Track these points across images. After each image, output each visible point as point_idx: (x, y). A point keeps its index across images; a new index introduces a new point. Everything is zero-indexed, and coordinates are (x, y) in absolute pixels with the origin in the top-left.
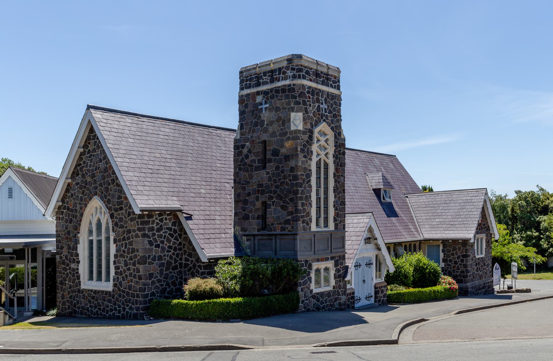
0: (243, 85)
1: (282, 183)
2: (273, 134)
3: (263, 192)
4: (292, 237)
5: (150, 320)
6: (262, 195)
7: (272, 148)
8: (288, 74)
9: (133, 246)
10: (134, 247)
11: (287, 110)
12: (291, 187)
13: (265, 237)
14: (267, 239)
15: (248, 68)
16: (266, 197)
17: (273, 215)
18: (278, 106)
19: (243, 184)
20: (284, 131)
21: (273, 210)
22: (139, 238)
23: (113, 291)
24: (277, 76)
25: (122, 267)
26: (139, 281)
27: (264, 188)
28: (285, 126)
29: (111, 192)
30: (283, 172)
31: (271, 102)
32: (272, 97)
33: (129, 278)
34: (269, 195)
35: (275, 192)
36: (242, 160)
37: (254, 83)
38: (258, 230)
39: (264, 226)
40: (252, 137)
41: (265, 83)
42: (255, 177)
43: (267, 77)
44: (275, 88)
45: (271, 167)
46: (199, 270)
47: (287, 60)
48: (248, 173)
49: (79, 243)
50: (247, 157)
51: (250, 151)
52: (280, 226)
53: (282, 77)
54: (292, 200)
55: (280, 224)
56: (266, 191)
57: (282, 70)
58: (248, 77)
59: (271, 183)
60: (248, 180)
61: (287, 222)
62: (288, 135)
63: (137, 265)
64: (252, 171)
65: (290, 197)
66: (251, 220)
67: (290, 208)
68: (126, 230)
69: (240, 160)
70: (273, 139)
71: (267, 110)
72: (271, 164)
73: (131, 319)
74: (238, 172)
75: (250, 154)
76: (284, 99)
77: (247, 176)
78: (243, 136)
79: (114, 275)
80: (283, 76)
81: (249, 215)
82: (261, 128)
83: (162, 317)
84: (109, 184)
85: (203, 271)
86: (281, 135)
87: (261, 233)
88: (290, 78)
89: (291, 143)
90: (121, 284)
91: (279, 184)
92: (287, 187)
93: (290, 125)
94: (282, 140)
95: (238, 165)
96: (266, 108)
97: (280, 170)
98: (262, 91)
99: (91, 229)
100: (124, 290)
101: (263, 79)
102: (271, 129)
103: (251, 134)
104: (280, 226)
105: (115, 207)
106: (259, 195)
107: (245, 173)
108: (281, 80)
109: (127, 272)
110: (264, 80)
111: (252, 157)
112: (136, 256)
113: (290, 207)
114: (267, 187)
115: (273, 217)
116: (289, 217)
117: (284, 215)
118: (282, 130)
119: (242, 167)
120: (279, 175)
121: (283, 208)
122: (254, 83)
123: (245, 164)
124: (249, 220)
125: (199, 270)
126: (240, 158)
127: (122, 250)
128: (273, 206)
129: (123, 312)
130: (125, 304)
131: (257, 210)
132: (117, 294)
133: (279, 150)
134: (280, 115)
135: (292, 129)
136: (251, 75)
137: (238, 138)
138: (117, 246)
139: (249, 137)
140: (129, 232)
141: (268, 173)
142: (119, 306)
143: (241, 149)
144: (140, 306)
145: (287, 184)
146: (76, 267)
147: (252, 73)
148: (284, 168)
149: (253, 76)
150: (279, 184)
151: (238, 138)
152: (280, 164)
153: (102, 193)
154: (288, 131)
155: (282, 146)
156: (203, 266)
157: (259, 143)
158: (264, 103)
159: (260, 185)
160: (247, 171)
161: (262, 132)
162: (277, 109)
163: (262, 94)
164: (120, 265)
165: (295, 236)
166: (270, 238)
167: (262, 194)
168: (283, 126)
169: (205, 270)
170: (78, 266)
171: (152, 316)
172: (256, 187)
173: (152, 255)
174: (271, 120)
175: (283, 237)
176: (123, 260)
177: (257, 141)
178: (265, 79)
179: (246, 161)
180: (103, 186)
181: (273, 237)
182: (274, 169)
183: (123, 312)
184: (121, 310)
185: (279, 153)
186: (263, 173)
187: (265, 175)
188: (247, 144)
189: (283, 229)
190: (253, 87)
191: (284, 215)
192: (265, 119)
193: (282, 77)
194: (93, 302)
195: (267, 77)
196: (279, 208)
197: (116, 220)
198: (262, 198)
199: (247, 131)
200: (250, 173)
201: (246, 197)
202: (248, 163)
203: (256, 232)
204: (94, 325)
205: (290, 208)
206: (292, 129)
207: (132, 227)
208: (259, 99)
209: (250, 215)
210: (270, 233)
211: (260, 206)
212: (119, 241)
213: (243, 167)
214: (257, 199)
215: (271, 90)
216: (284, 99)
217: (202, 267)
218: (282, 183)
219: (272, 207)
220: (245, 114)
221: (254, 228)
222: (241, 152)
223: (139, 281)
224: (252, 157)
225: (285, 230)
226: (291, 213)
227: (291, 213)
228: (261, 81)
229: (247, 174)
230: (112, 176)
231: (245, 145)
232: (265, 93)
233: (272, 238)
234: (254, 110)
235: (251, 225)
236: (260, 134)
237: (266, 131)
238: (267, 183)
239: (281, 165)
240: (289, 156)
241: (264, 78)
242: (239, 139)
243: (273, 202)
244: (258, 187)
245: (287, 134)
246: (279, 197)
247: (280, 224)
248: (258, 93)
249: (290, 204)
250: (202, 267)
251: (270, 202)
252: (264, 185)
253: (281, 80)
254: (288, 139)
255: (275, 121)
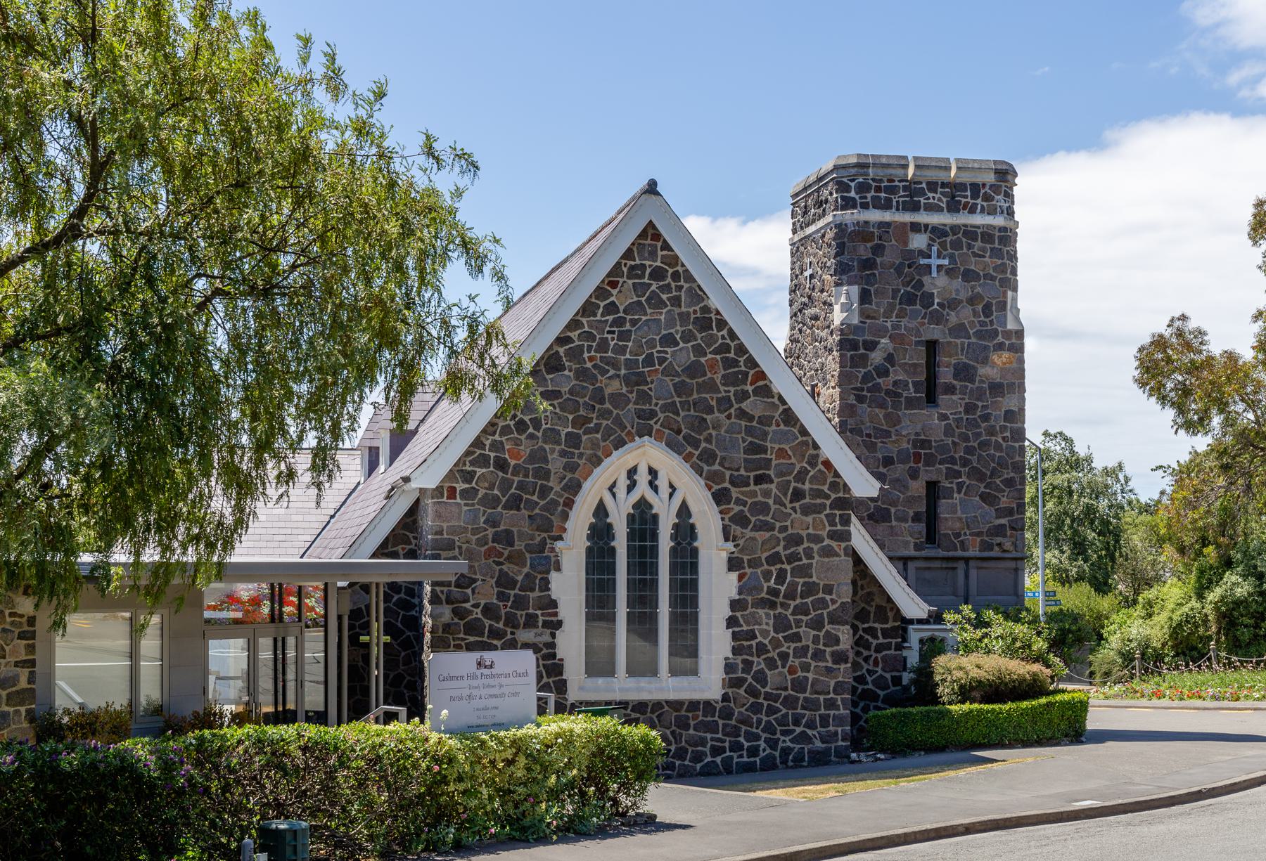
0: (866, 198)
1: (984, 445)
2: (959, 330)
3: (930, 460)
4: (1012, 564)
5: (877, 759)
6: (928, 466)
7: (953, 362)
8: (999, 204)
9: (811, 577)
10: (814, 579)
11: (997, 283)
12: (1007, 455)
13: (937, 564)
14: (942, 568)
15: (884, 161)
16: (939, 471)
17: (959, 514)
18: (973, 267)
19: (869, 436)
20: (989, 328)
21: (958, 501)
22: (838, 559)
23: (725, 698)
24: (969, 200)
25: (765, 633)
26: (835, 666)
27: (933, 451)
28: (993, 317)
29: (714, 433)
30: (986, 418)
31: (951, 257)
32: (957, 245)
33: (793, 661)
34: (947, 468)
35: (965, 463)
36: (867, 377)
37: (901, 199)
38: (918, 547)
39: (932, 536)
40: (896, 327)
41: (931, 208)
42: (905, 422)
43: (939, 195)
44: (965, 226)
45: (951, 404)
46: (871, 640)
47: (997, 172)
48: (883, 411)
49: (558, 569)
50: (883, 372)
51: (890, 358)
52: (979, 539)
53: (982, 206)
54: (1009, 483)
55: (979, 534)
56: (939, 457)
57: (983, 191)
58: (881, 181)
59: (953, 442)
60: (885, 428)
61: (999, 531)
62: (1000, 339)
63: (828, 627)
64: (896, 406)
65: (1006, 476)
66: (894, 523)
67: (1005, 502)
68: (781, 536)
69: (860, 376)
70: (958, 341)
71: (943, 273)
72: (954, 397)
73: (803, 766)
74: (852, 406)
75: (893, 366)
76: (991, 257)
77: (881, 416)
78: (868, 321)
79: (730, 655)
80: (985, 204)
81: (888, 510)
82: (924, 311)
83: (915, 750)
84: (710, 410)
85: (881, 640)
86: (979, 335)
87: (924, 553)
88: (1002, 212)
89: (1009, 358)
90: (761, 678)
91: (976, 445)
92: (998, 454)
93: (1005, 316)
94: (986, 348)
95: (852, 389)
96: (939, 267)
97: (979, 414)
98: (926, 226)
99: (882, 527)
100: (774, 692)
101: (928, 198)
102: (953, 319)
103: (894, 319)
104: (979, 539)
105: (736, 473)
106: (920, 465)
107: (877, 410)
108: (978, 210)
109: (786, 645)
110: (931, 201)
111: (897, 374)
112: (822, 604)
113: (1005, 499)
114: (943, 448)
115: (960, 519)
116: (1003, 521)
117: (987, 516)
118: (982, 324)
119: (865, 393)
120: (972, 424)
121: (984, 497)
122: (901, 199)
123: (876, 388)
124: (891, 521)
125: (871, 640)
126: (860, 372)
127: (765, 589)
128: (959, 492)
129: (768, 751)
130: (779, 728)
131: (911, 500)
132: (744, 705)
133: (975, 369)
134: (979, 290)
135: (1009, 327)
136: (894, 181)
137: (856, 321)
138: (740, 578)
139: (889, 324)
140: (795, 540)
141: (944, 417)
142: (752, 737)
143: (862, 351)
144: (840, 730)
145: (998, 447)
146: (547, 638)
147: (896, 176)
148: (989, 411)
149: (897, 183)
150: (976, 445)
151: (856, 321)
152: (978, 399)
153: (679, 432)
154: (1000, 329)
155: (985, 361)
156: (881, 629)
157: (918, 343)
158: (934, 254)
159: (925, 443)
160: (882, 406)
161: (926, 321)
162: (968, 276)
163: (925, 232)
164: (756, 627)
165: (1019, 562)
166: (950, 565)
167: (927, 464)
168: (987, 316)
169: (890, 640)
170: (553, 635)
171: (882, 751)
172: (910, 446)
173: (833, 602)
174: (954, 296)
175: (985, 564)
176: (767, 615)
177: (913, 338)
178: (934, 198)
179: (880, 381)
180: (682, 414)
181: (961, 566)
182: (961, 409)
183: (768, 751)
184: (759, 746)
185: (974, 375)
186: (930, 416)
187: (936, 422)
188: (883, 341)
189: (987, 546)
190: (898, 209)
191: (987, 516)
192: (935, 291)
193: (982, 206)
194: (759, 721)
195: (939, 195)
196: (977, 498)
197: (737, 509)
198: (927, 474)
199: (882, 310)
200: (890, 410)
201: (878, 467)
202: (884, 387)
203: (912, 553)
204: (874, 775)
205: (1005, 502)
206: (1009, 327)
207: (808, 528)
208: (918, 241)
209: (893, 510)
210: (951, 554)
211: (923, 492)
212: (754, 563)
213: (869, 395)
214: (914, 475)
215: (955, 229)
216: (991, 257)
217: (879, 631)
218: (984, 445)
219: (955, 495)
220: (876, 268)
221: (907, 543)
222: (864, 358)
223: (835, 666)
224: (897, 374)
225: (992, 550)
226: (1001, 513)
227: (1001, 513)
228: (922, 200)
229: (881, 413)
230: (722, 388)
231: (878, 343)
232: (937, 232)
233: (955, 565)
234: (901, 264)
235: (897, 535)
236: (923, 324)
237: (937, 319)
238: (942, 440)
239: (980, 404)
240: (1000, 385)
241: (931, 195)
242: (856, 327)
243: (960, 486)
244: (915, 446)
245: (997, 336)
246: (978, 475)
247: (979, 534)
248: (916, 227)
249: (1004, 491)
250: (879, 631)
251: (952, 483)
252: (933, 444)
253: (978, 210)
254: (1000, 347)
255: (962, 301)
